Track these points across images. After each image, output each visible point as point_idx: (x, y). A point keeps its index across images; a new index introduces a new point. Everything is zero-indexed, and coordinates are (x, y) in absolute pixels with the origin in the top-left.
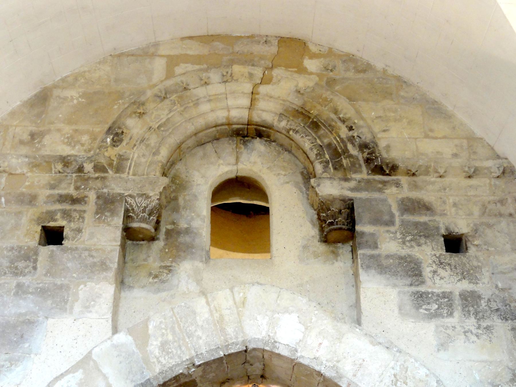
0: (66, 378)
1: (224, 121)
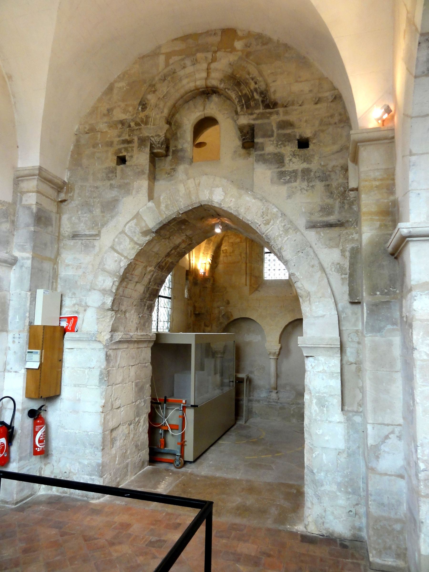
0: (130, 222)
1: (194, 88)
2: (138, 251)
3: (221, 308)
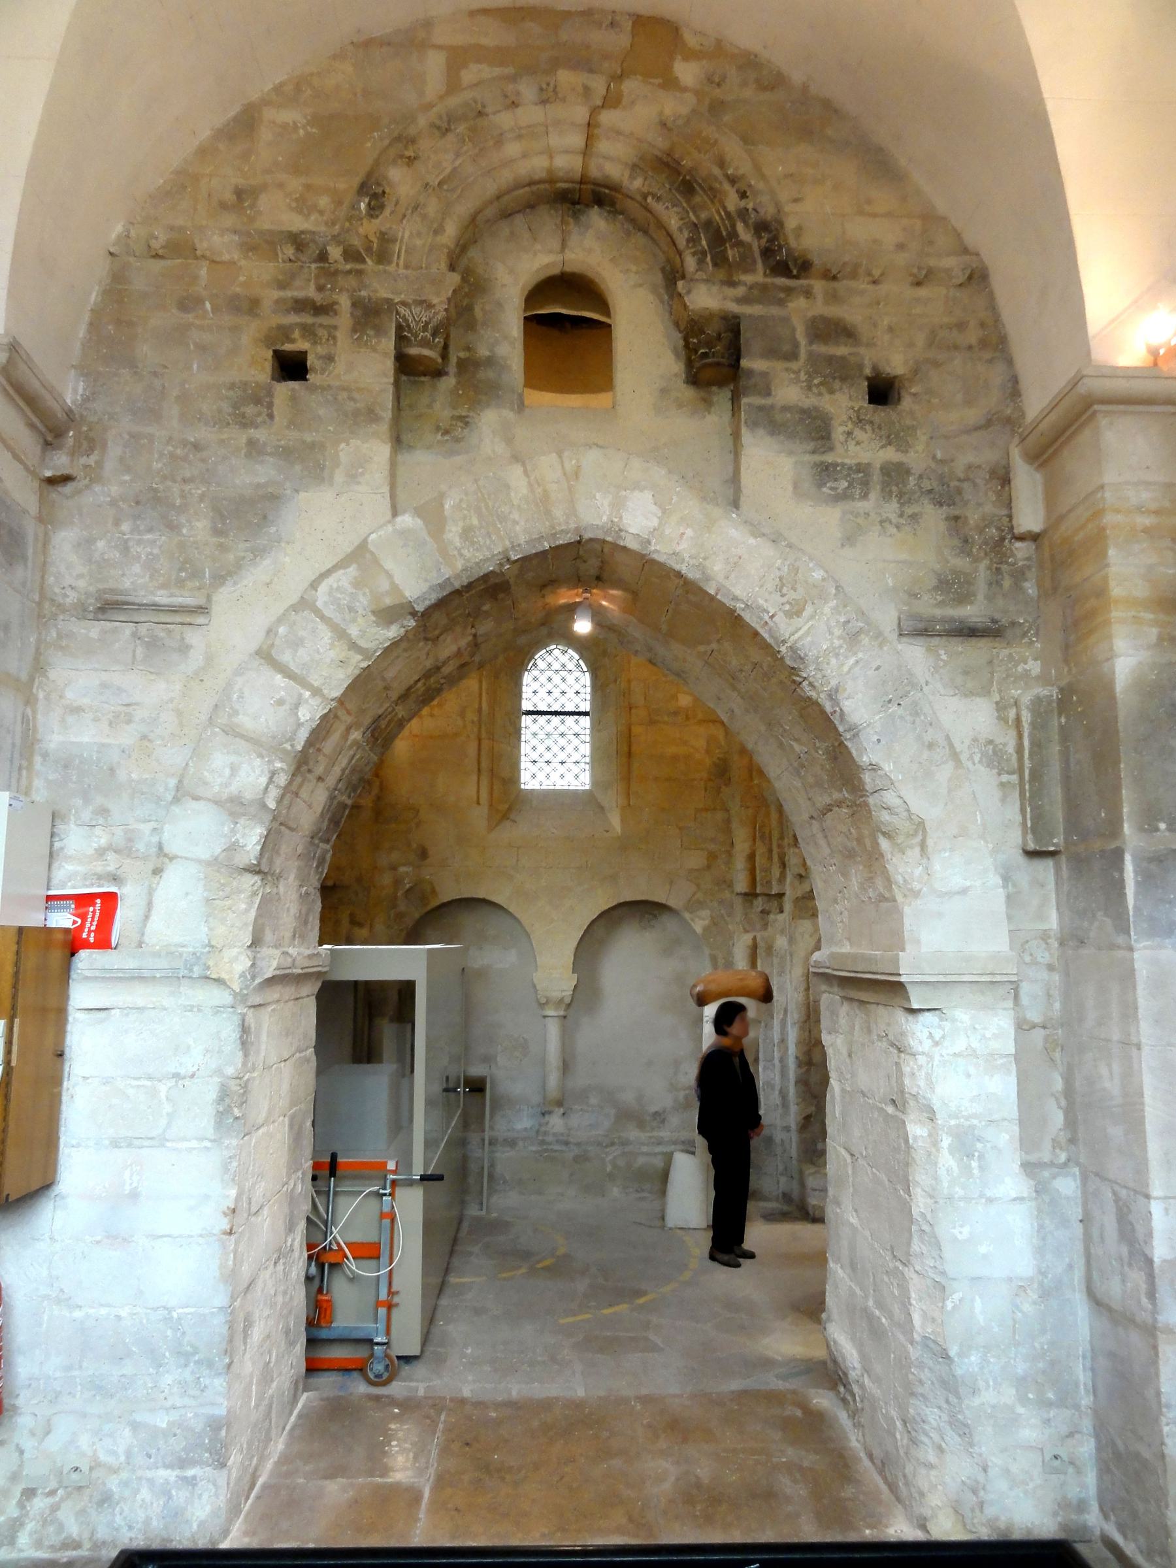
1: (544, 175)
2: (357, 672)
3: (402, 869)
